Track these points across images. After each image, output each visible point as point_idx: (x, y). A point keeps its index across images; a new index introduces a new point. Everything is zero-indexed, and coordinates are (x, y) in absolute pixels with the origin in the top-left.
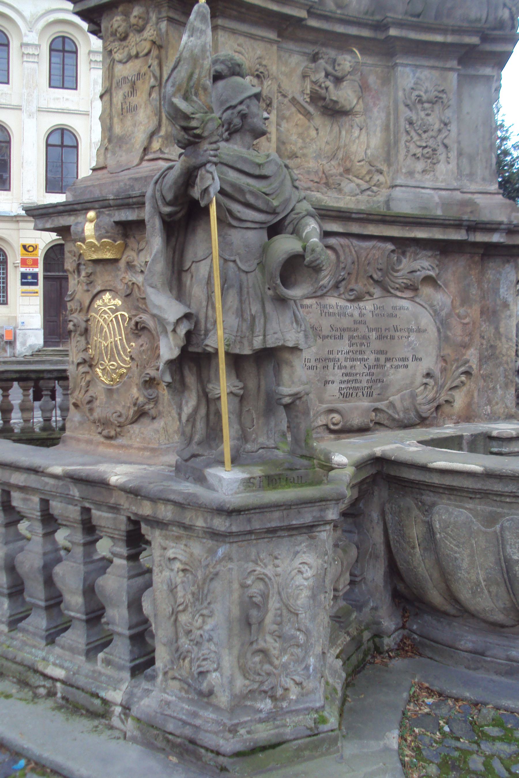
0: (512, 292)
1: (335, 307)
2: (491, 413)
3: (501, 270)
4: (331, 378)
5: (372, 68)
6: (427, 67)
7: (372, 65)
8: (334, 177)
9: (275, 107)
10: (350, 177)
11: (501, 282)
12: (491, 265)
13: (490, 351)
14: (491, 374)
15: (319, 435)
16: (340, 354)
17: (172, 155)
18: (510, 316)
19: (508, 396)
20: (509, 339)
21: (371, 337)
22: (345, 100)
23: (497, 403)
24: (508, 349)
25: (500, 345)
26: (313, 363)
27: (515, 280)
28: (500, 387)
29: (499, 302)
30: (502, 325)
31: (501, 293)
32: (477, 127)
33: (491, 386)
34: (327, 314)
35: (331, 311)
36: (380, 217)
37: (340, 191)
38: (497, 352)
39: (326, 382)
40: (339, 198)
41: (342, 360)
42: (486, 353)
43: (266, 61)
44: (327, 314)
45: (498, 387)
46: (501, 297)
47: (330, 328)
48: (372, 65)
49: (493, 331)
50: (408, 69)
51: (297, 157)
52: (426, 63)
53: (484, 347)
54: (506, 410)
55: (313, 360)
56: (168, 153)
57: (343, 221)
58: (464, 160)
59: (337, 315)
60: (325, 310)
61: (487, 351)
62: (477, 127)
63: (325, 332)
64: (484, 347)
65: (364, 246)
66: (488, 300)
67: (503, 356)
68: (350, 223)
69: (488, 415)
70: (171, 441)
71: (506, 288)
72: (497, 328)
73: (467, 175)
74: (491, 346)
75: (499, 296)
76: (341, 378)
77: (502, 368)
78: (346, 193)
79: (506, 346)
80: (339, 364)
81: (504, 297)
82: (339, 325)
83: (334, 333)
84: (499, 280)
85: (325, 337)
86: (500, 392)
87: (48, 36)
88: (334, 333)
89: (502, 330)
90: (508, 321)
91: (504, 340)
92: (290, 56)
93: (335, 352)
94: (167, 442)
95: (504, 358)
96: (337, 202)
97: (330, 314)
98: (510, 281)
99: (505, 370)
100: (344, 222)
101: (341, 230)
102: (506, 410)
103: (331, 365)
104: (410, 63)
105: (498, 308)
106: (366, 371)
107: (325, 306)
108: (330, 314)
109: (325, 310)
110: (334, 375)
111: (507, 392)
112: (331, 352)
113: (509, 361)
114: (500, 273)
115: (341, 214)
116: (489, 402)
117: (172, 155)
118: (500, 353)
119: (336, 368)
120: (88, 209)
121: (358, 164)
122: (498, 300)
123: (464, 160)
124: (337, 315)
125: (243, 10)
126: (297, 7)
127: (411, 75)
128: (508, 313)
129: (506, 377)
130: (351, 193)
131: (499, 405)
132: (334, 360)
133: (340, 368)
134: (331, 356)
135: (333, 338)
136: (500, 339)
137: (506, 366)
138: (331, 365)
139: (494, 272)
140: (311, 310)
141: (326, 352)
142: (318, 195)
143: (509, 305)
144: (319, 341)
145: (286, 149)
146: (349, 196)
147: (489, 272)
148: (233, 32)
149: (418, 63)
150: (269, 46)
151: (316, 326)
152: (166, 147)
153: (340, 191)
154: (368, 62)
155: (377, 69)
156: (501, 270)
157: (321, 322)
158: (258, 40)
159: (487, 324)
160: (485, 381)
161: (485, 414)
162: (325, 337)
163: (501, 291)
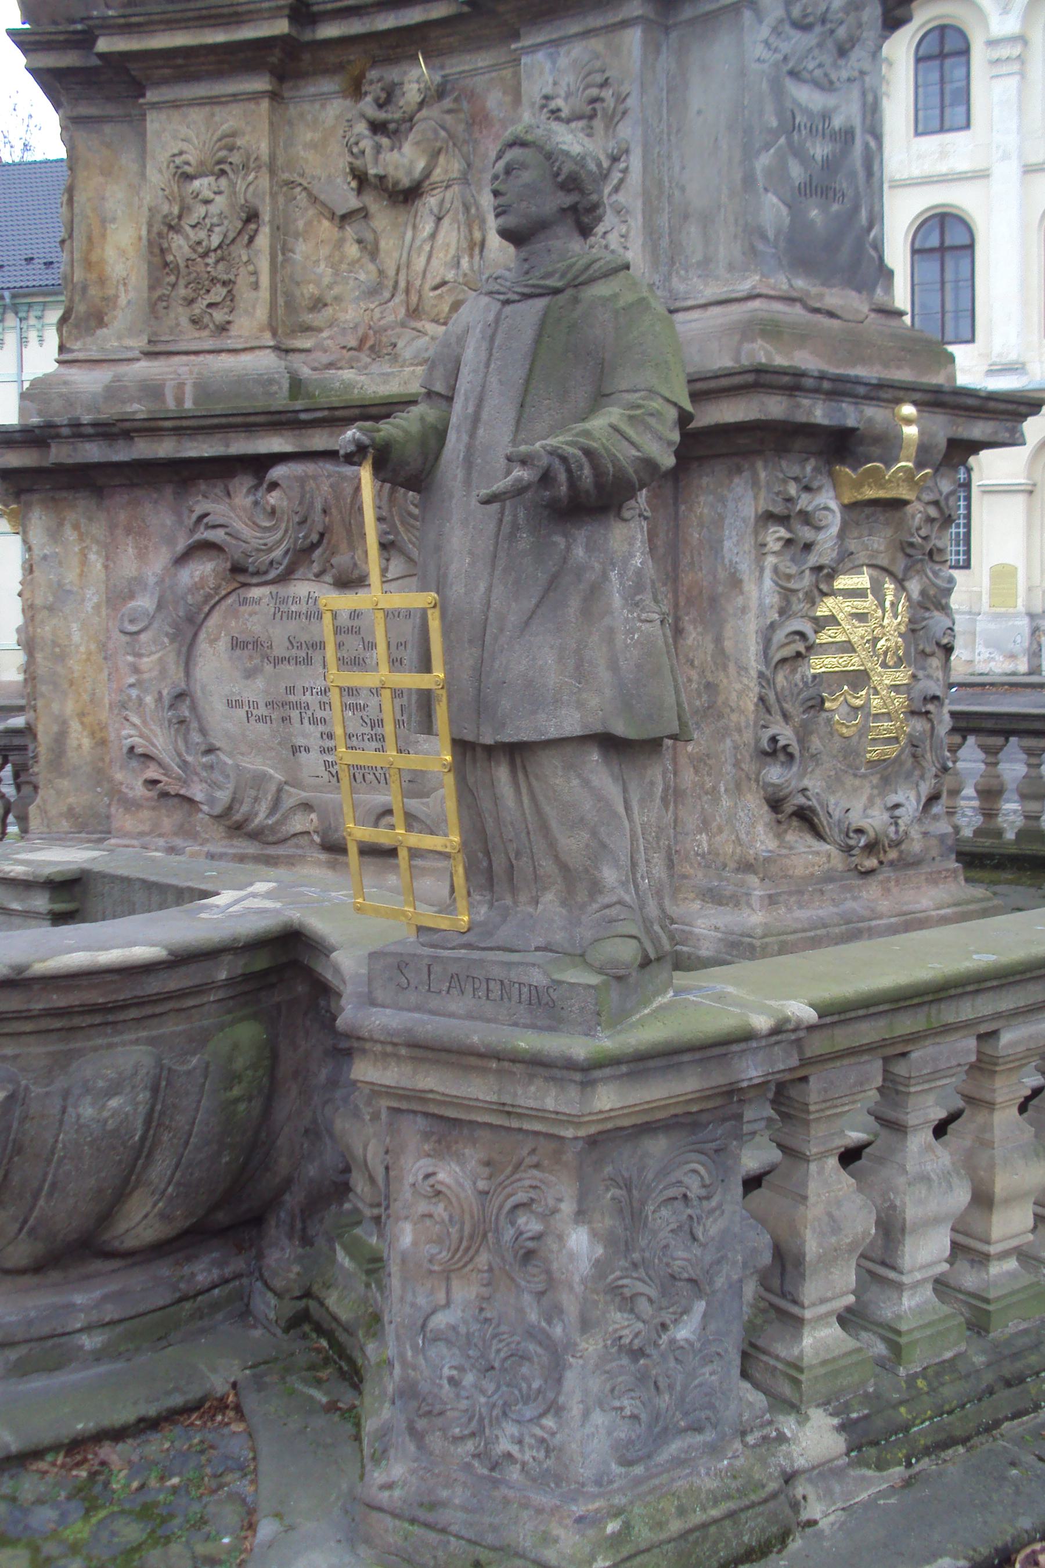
0: (746, 547)
1: (304, 602)
2: (709, 853)
3: (726, 492)
4: (300, 741)
5: (494, 74)
6: (576, 35)
7: (491, 68)
8: (389, 332)
9: (267, 218)
10: (419, 325)
11: (727, 522)
12: (705, 481)
13: (705, 698)
14: (708, 756)
15: (300, 852)
16: (308, 693)
17: (90, 350)
18: (744, 610)
19: (741, 814)
20: (742, 669)
21: (368, 661)
22: (396, 168)
23: (720, 830)
24: (740, 694)
25: (725, 681)
26: (262, 711)
27: (753, 515)
28: (726, 790)
29: (722, 575)
30: (728, 632)
31: (725, 549)
32: (716, 140)
33: (709, 785)
34: (285, 616)
35: (294, 608)
36: (357, 411)
37: (395, 358)
38: (720, 700)
39: (295, 750)
40: (388, 374)
41: (315, 706)
42: (698, 703)
43: (247, 138)
44: (285, 616)
45: (722, 789)
46: (727, 561)
47: (287, 644)
48: (491, 68)
49: (711, 646)
50: (540, 56)
51: (326, 305)
52: (574, 28)
53: (694, 686)
54: (738, 850)
55: (261, 705)
56: (79, 350)
57: (293, 429)
58: (693, 229)
59: (303, 617)
60: (283, 608)
61: (700, 696)
62: (716, 140)
63: (279, 651)
64: (694, 686)
65: (349, 474)
66: (701, 569)
67: (732, 711)
68: (310, 431)
69: (703, 856)
70: (54, 829)
71: (735, 539)
72: (718, 640)
73: (699, 264)
74: (709, 686)
75: (723, 558)
76: (321, 743)
77: (728, 742)
78: (405, 360)
79: (738, 686)
80: (309, 713)
81: (731, 561)
82: (304, 637)
83: (294, 652)
84: (722, 518)
85: (278, 661)
86: (726, 802)
87: (904, 49)
88: (294, 652)
89: (728, 644)
90: (740, 622)
91: (732, 668)
92: (323, 106)
93: (299, 690)
94: (46, 830)
95: (734, 717)
96: (385, 382)
97: (291, 616)
98: (744, 520)
99: (736, 748)
100: (297, 432)
101: (288, 448)
102: (738, 850)
103: (295, 714)
104: (540, 40)
105: (720, 589)
106: (367, 730)
107: (284, 601)
108: (291, 616)
109: (283, 608)
110: (305, 736)
111: (739, 805)
112: (291, 690)
113: (743, 724)
114: (723, 500)
115: (276, 417)
116: (705, 825)
117: (90, 350)
118: (726, 703)
119: (306, 721)
120: (899, 401)
121: (431, 294)
122: (720, 570)
123: (693, 229)
124: (303, 617)
125: (180, 61)
126: (265, 19)
127: (548, 66)
128: (740, 601)
129: (737, 764)
130: (415, 357)
131: (724, 835)
132: (297, 705)
133: (313, 721)
134: (292, 698)
135: (293, 662)
136: (725, 667)
137: (736, 737)
138: (295, 714)
139: (711, 498)
140: (257, 608)
141: (282, 690)
142: (348, 374)
143: (741, 581)
144: (268, 668)
145: (302, 294)
146: (412, 365)
147: (702, 499)
148: (176, 105)
149: (554, 36)
150: (252, 106)
151: (262, 639)
152: (77, 339)
153: (395, 358)
154: (480, 64)
155: (504, 72)
156: (726, 492)
157: (271, 631)
158: (227, 103)
159: (700, 629)
160: (696, 771)
161: (697, 854)
162: (278, 661)
163: (727, 544)
